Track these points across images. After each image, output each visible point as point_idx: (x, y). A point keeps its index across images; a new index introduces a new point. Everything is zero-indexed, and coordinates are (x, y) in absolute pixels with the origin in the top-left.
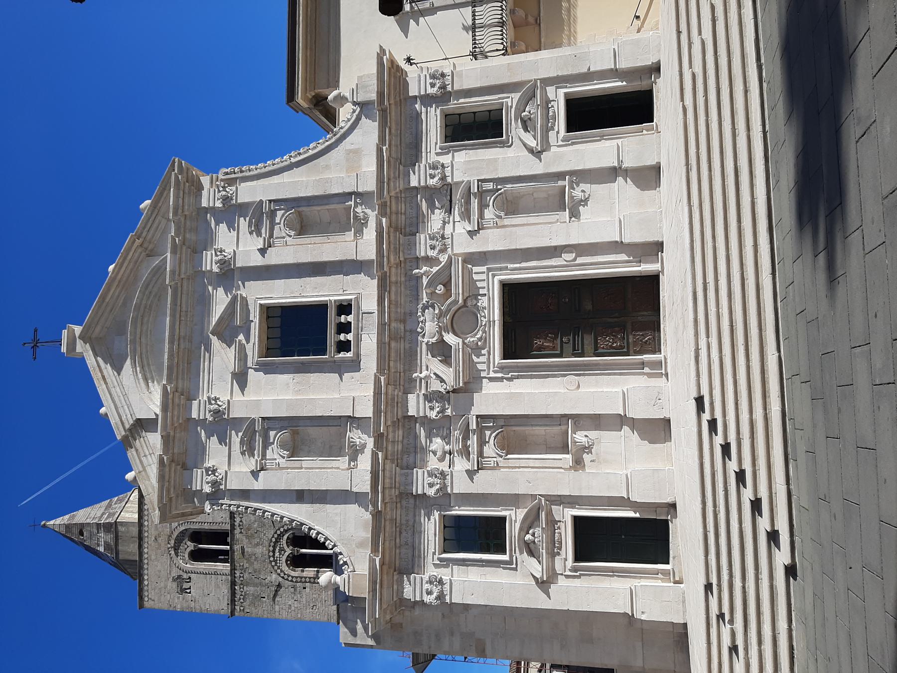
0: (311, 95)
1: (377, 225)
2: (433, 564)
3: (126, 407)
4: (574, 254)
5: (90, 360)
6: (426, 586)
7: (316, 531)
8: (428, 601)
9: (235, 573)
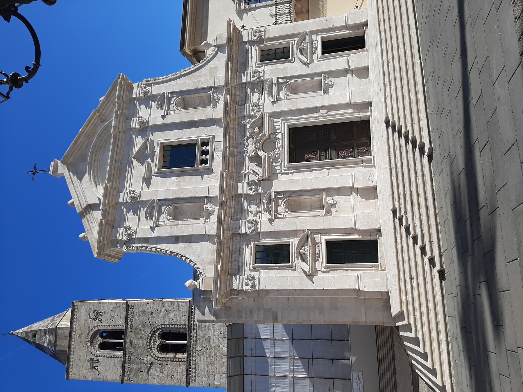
0: (192, 48)
1: (224, 98)
2: (250, 270)
3: (83, 197)
4: (326, 110)
5: (66, 173)
6: (245, 281)
7: (185, 257)
8: (246, 289)
9: (126, 356)
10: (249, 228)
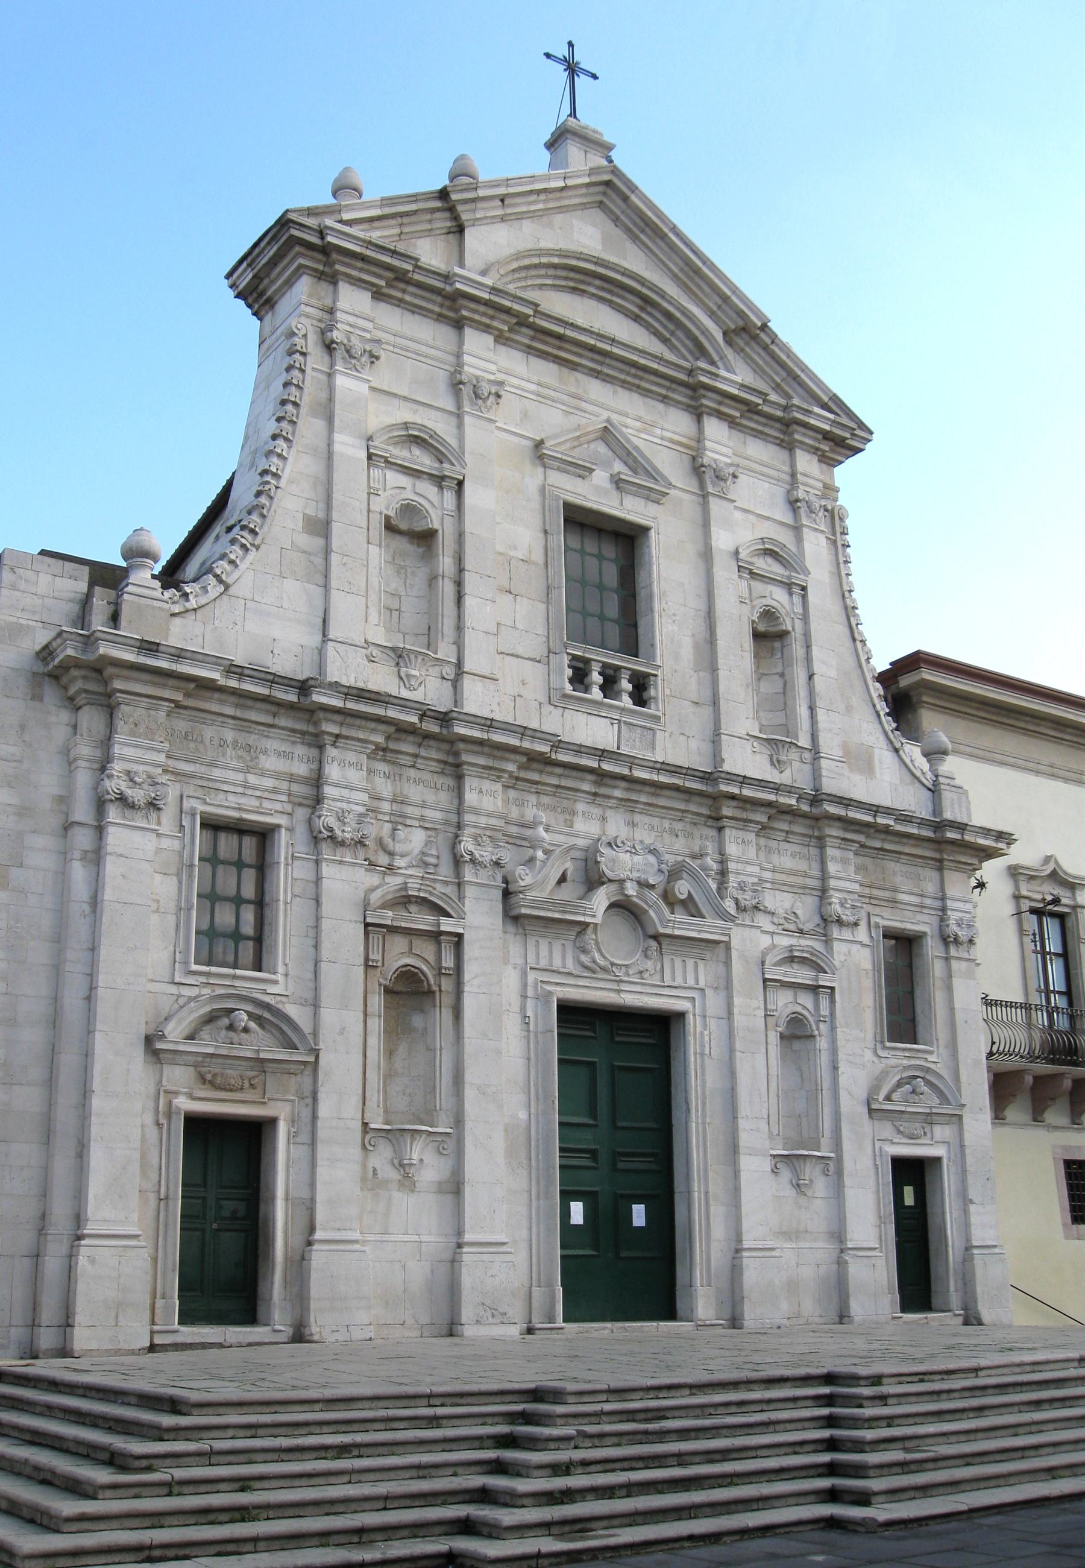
10: (341, 819)
